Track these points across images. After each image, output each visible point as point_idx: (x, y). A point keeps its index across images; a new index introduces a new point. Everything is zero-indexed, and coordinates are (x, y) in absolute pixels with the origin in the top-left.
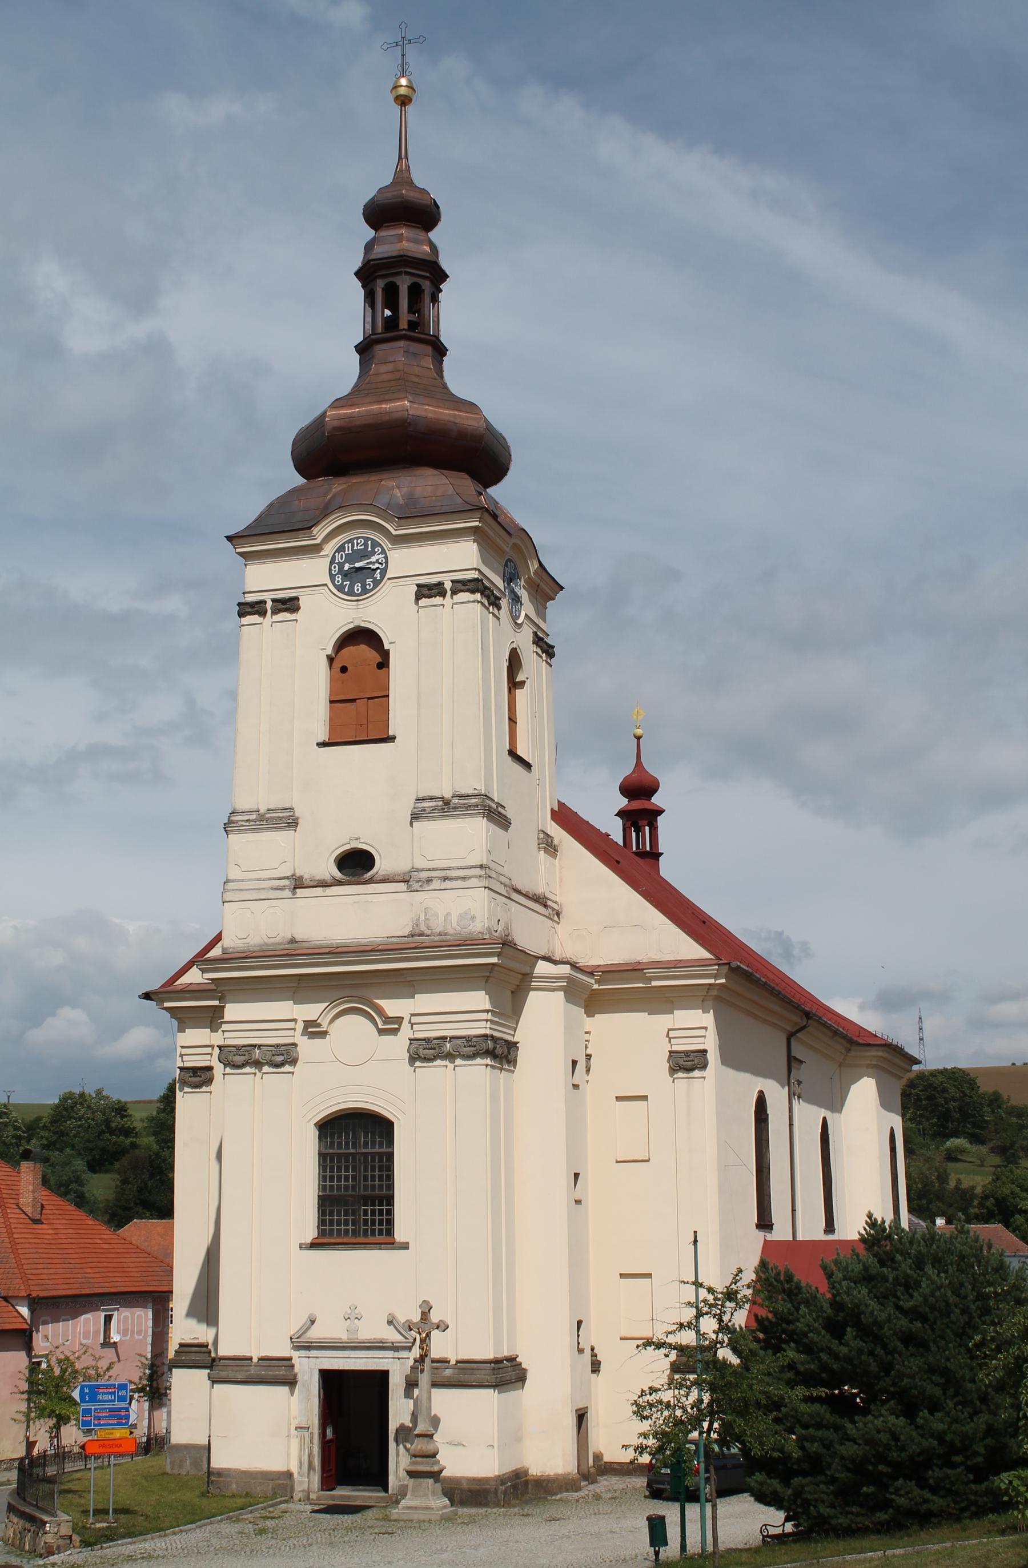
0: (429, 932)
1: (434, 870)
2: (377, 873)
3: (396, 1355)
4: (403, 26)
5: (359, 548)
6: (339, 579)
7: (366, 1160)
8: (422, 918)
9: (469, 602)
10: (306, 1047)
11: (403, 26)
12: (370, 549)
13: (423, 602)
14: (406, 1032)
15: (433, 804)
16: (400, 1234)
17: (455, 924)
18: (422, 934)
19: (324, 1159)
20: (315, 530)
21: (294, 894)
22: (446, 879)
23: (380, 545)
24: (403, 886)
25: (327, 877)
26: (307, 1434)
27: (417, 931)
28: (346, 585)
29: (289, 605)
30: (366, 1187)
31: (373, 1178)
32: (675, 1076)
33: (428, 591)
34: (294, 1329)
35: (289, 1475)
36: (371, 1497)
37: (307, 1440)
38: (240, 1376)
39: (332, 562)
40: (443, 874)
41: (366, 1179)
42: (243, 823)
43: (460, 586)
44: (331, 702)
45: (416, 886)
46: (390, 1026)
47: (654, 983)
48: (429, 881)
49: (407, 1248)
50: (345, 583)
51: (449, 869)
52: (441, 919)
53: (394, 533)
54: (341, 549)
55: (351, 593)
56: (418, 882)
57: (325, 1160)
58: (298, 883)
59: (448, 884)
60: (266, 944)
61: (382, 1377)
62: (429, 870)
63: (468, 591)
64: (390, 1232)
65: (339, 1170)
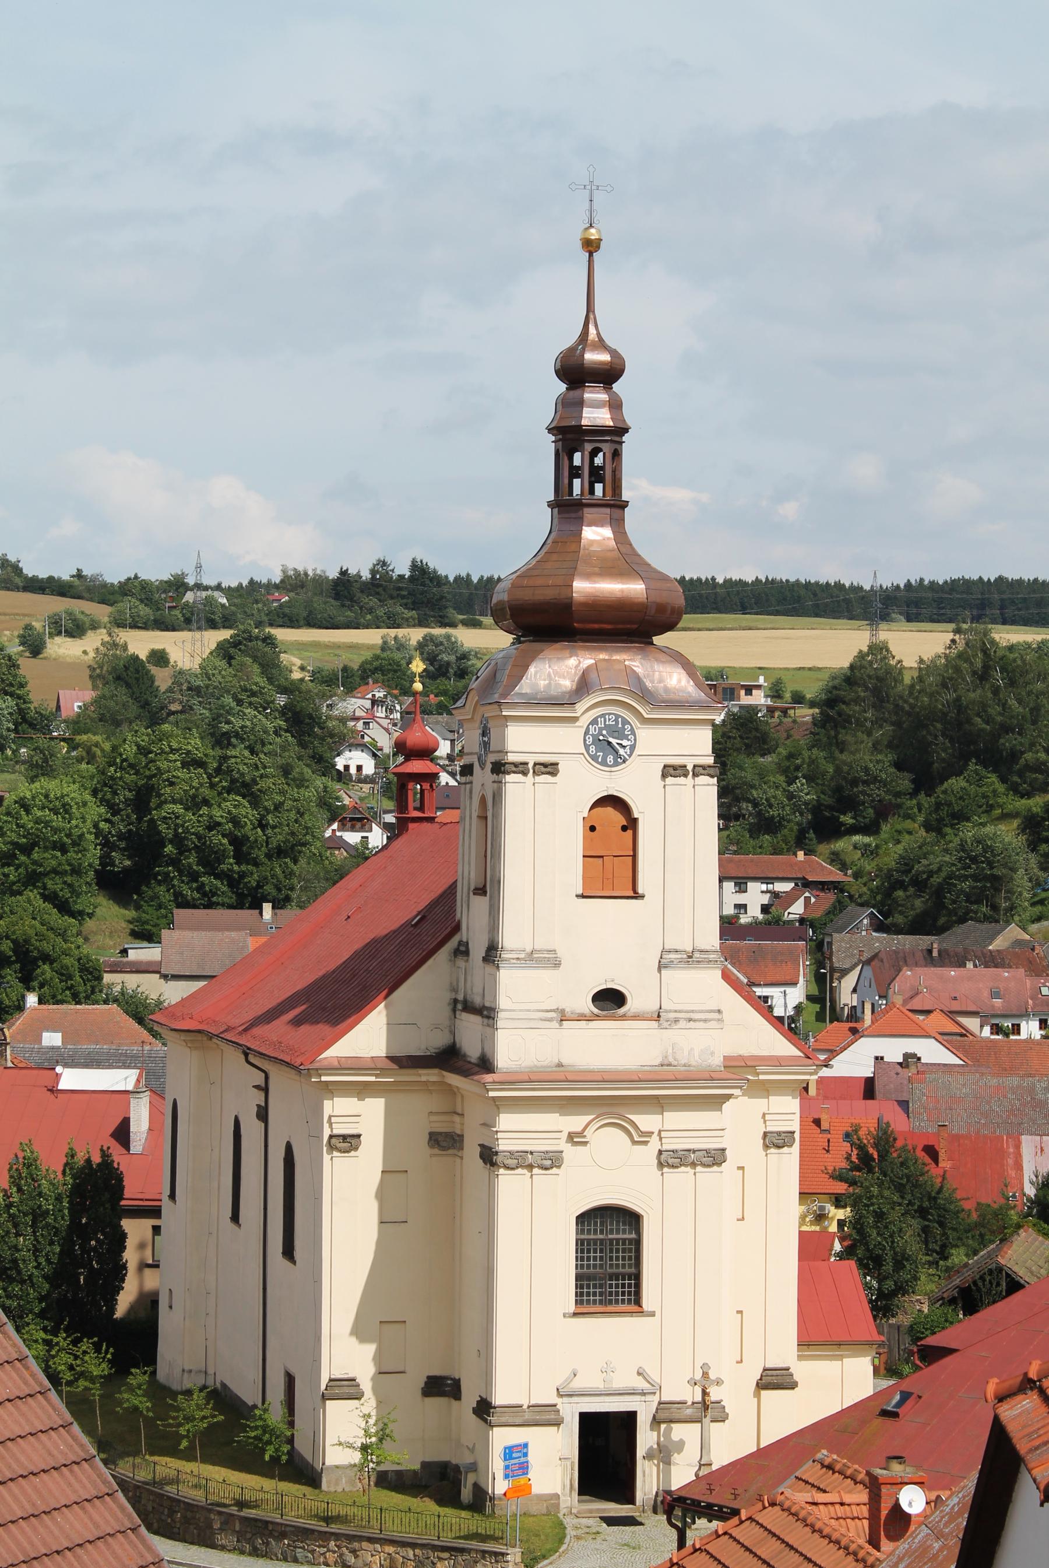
0: (676, 1063)
1: (680, 1011)
2: (629, 1010)
3: (643, 1398)
4: (573, 187)
6: (592, 749)
7: (611, 1244)
8: (670, 1051)
9: (709, 785)
10: (570, 1152)
11: (573, 187)
12: (620, 726)
13: (670, 780)
14: (654, 1145)
15: (679, 956)
16: (649, 1299)
17: (697, 1058)
18: (669, 1065)
19: (581, 1246)
20: (577, 706)
21: (561, 1025)
22: (690, 1020)
23: (629, 723)
24: (655, 1024)
25: (587, 1012)
26: (569, 1463)
27: (666, 1062)
29: (550, 768)
30: (611, 1266)
31: (617, 1258)
32: (768, 1152)
33: (671, 771)
34: (558, 1382)
35: (557, 1496)
36: (622, 1509)
37: (569, 1467)
38: (518, 1421)
39: (586, 733)
40: (688, 1015)
41: (611, 1259)
42: (515, 961)
43: (701, 770)
44: (584, 856)
45: (666, 1024)
46: (639, 1138)
47: (761, 1077)
48: (676, 1021)
49: (654, 1315)
51: (692, 1011)
52: (686, 1053)
53: (646, 716)
54: (594, 722)
55: (604, 763)
56: (667, 1021)
57: (582, 1244)
58: (563, 1017)
59: (692, 1024)
60: (536, 1066)
61: (629, 1419)
62: (676, 1011)
63: (709, 775)
64: (638, 1302)
65: (589, 1251)
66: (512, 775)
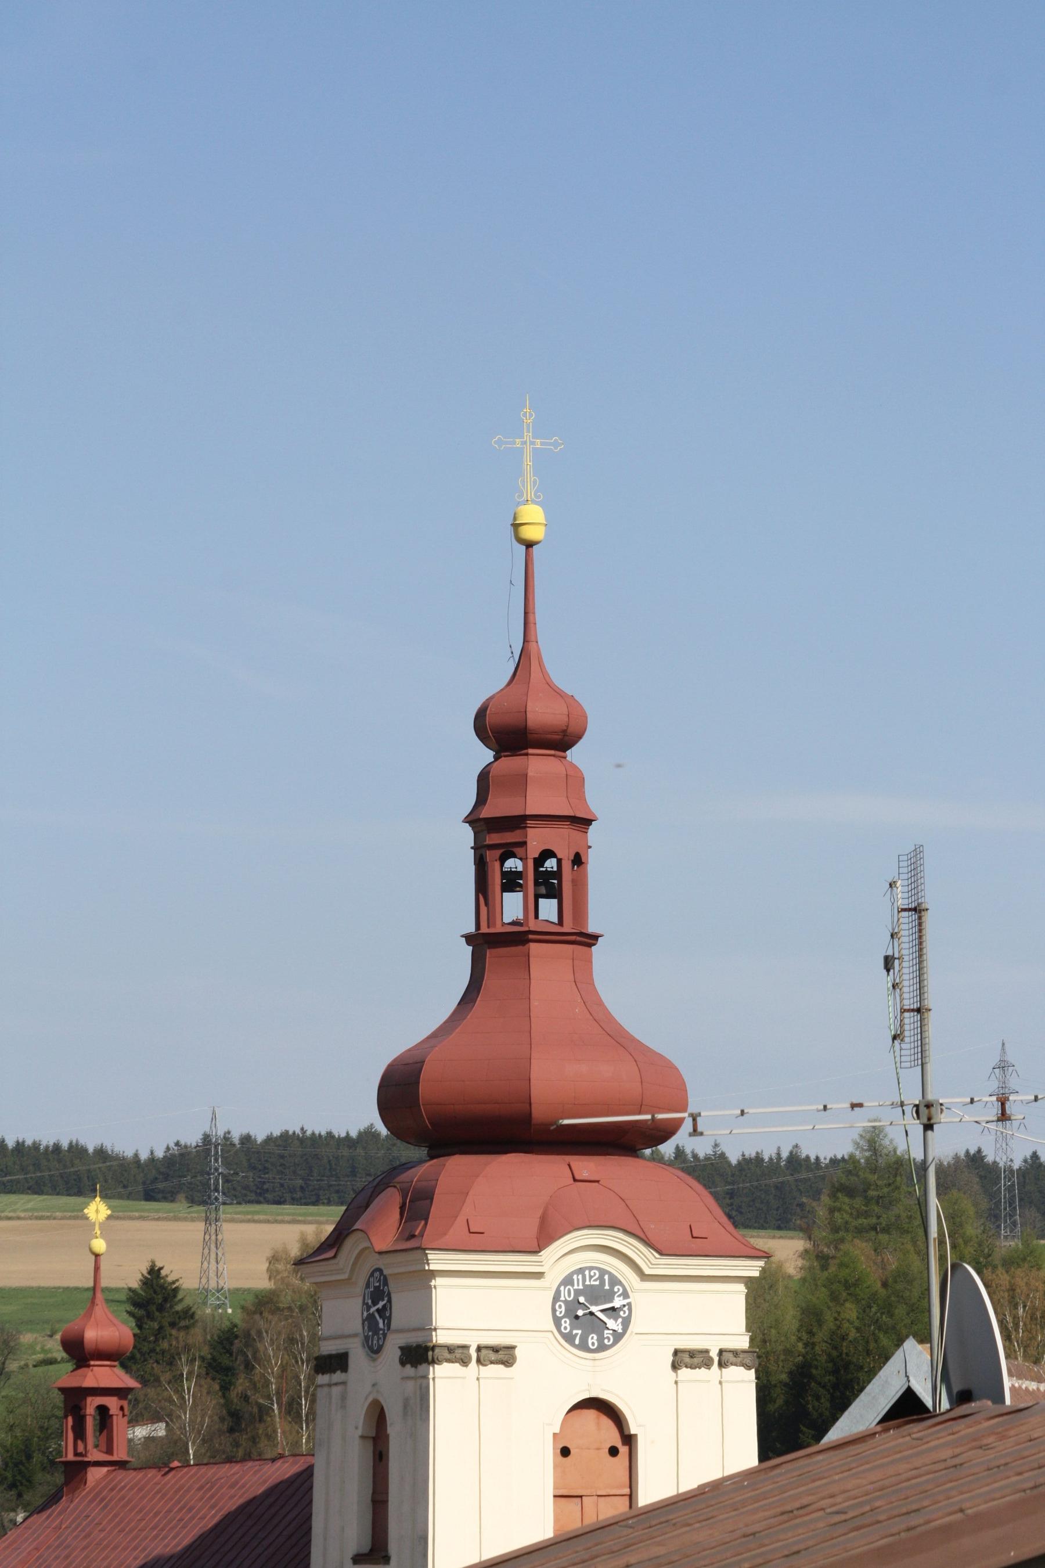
5: (593, 1283)
12: (607, 1287)
28: (577, 1334)
50: (575, 1332)
55: (584, 1347)
66: (445, 1364)
